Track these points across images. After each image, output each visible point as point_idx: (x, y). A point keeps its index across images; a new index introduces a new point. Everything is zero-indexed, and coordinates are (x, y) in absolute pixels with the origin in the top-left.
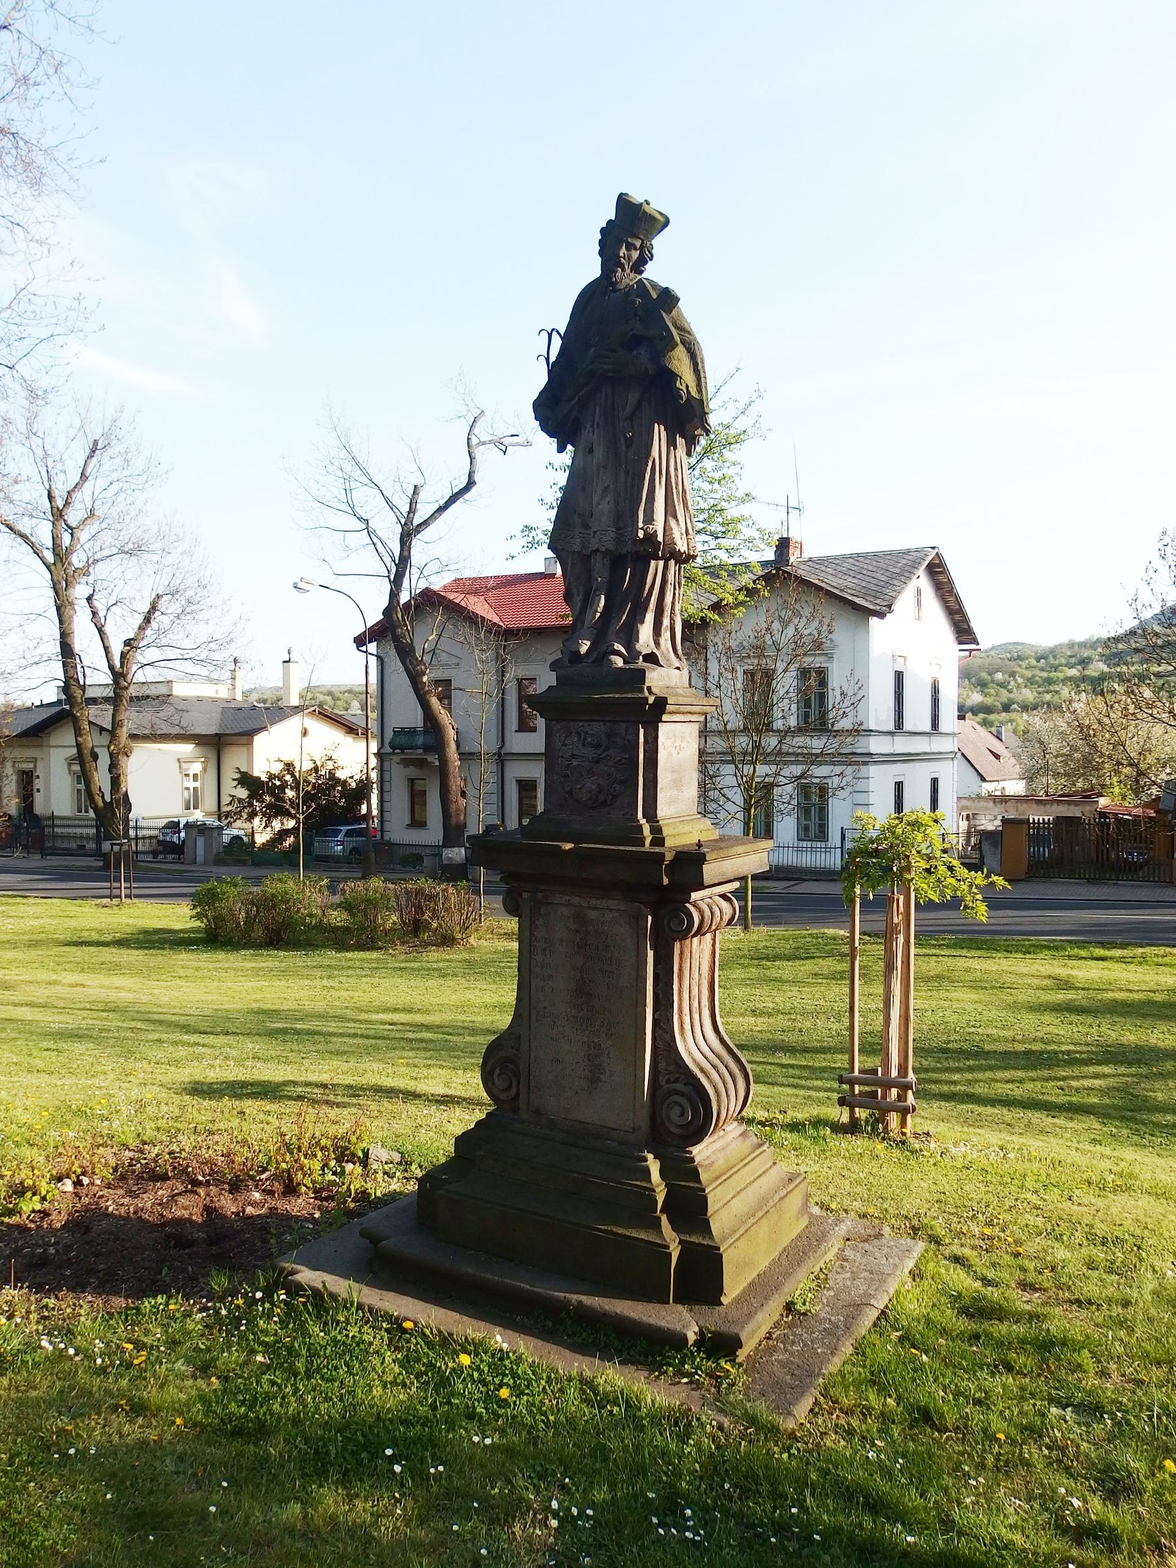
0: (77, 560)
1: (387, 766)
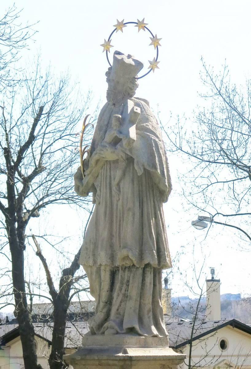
0: (29, 203)
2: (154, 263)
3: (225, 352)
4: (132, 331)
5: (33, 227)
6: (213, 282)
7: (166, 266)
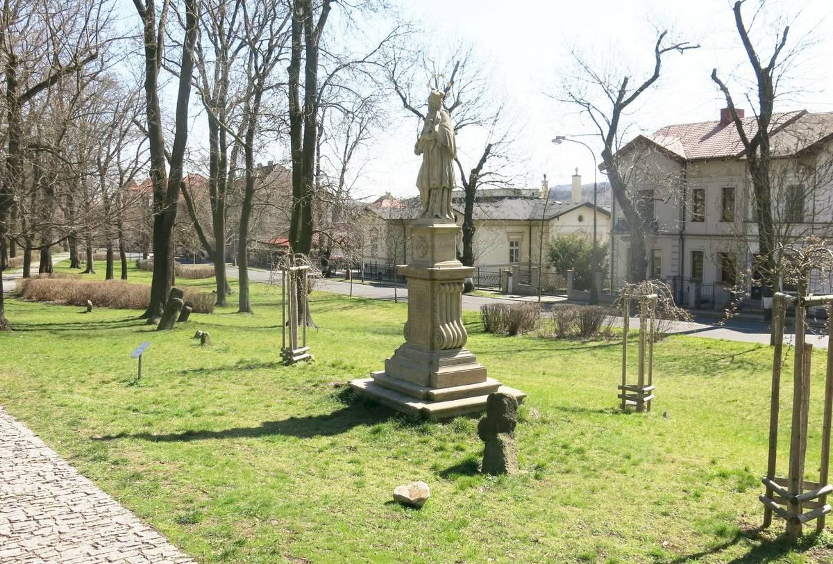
2: (448, 186)
3: (582, 224)
4: (437, 216)
6: (576, 176)
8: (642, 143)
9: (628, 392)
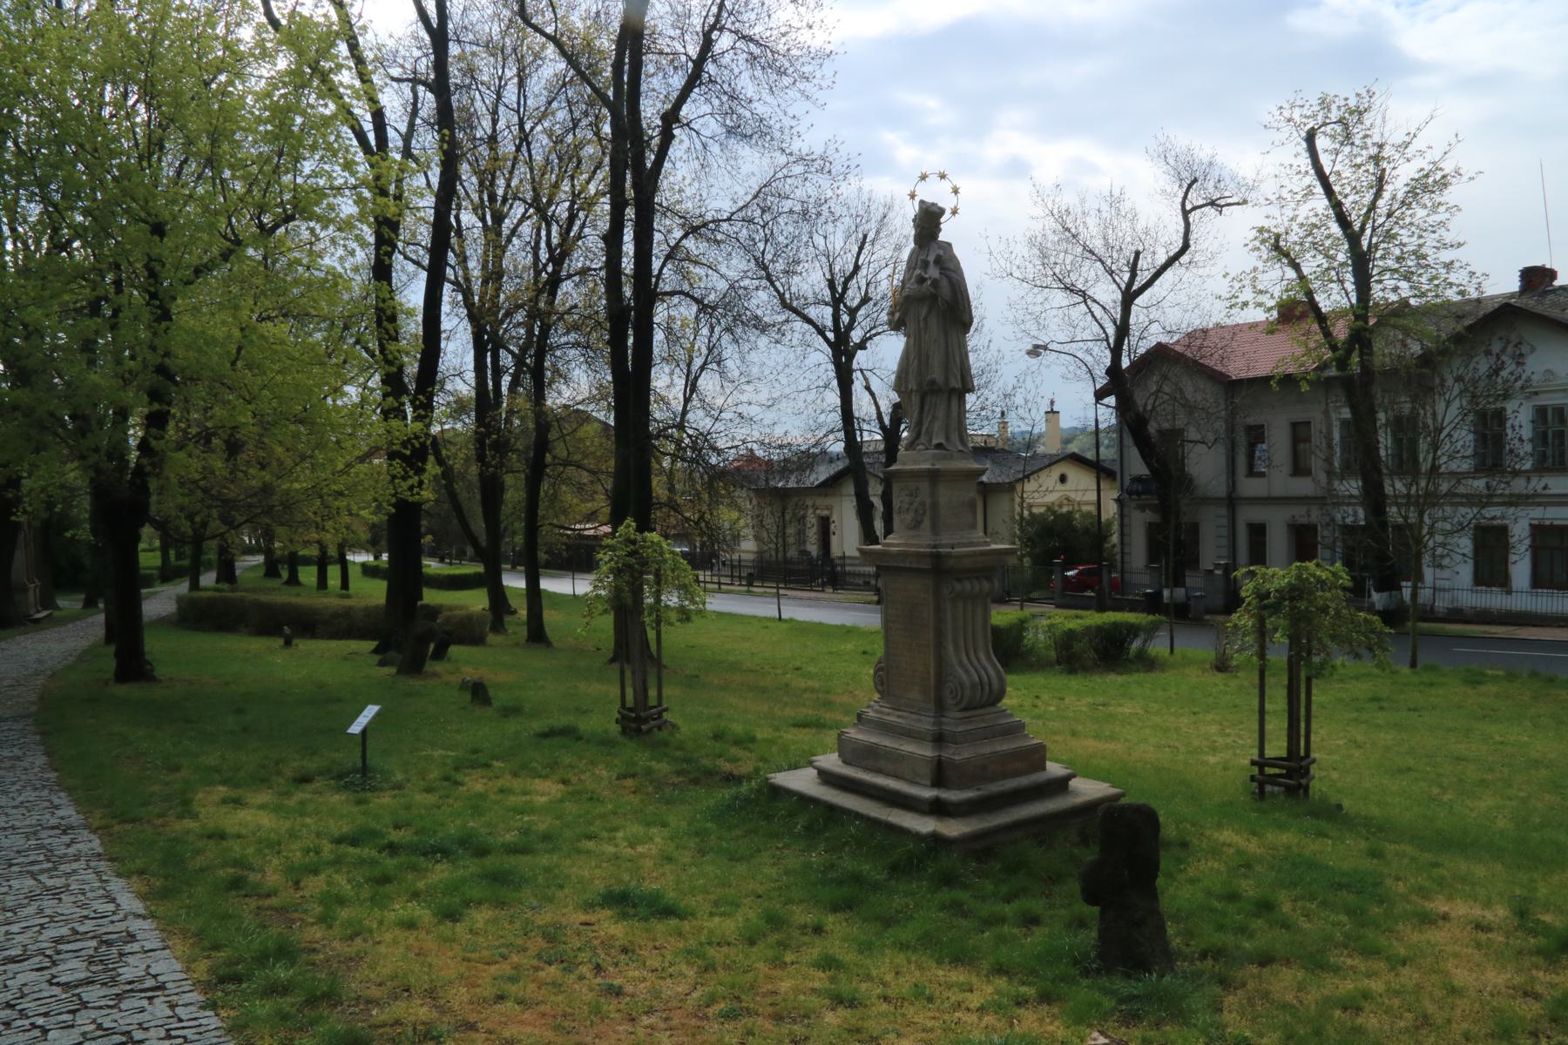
0: (856, 335)
1: (1126, 511)
5: (861, 359)
6: (1052, 413)
7: (971, 390)
8: (1160, 353)
9: (1270, 771)
